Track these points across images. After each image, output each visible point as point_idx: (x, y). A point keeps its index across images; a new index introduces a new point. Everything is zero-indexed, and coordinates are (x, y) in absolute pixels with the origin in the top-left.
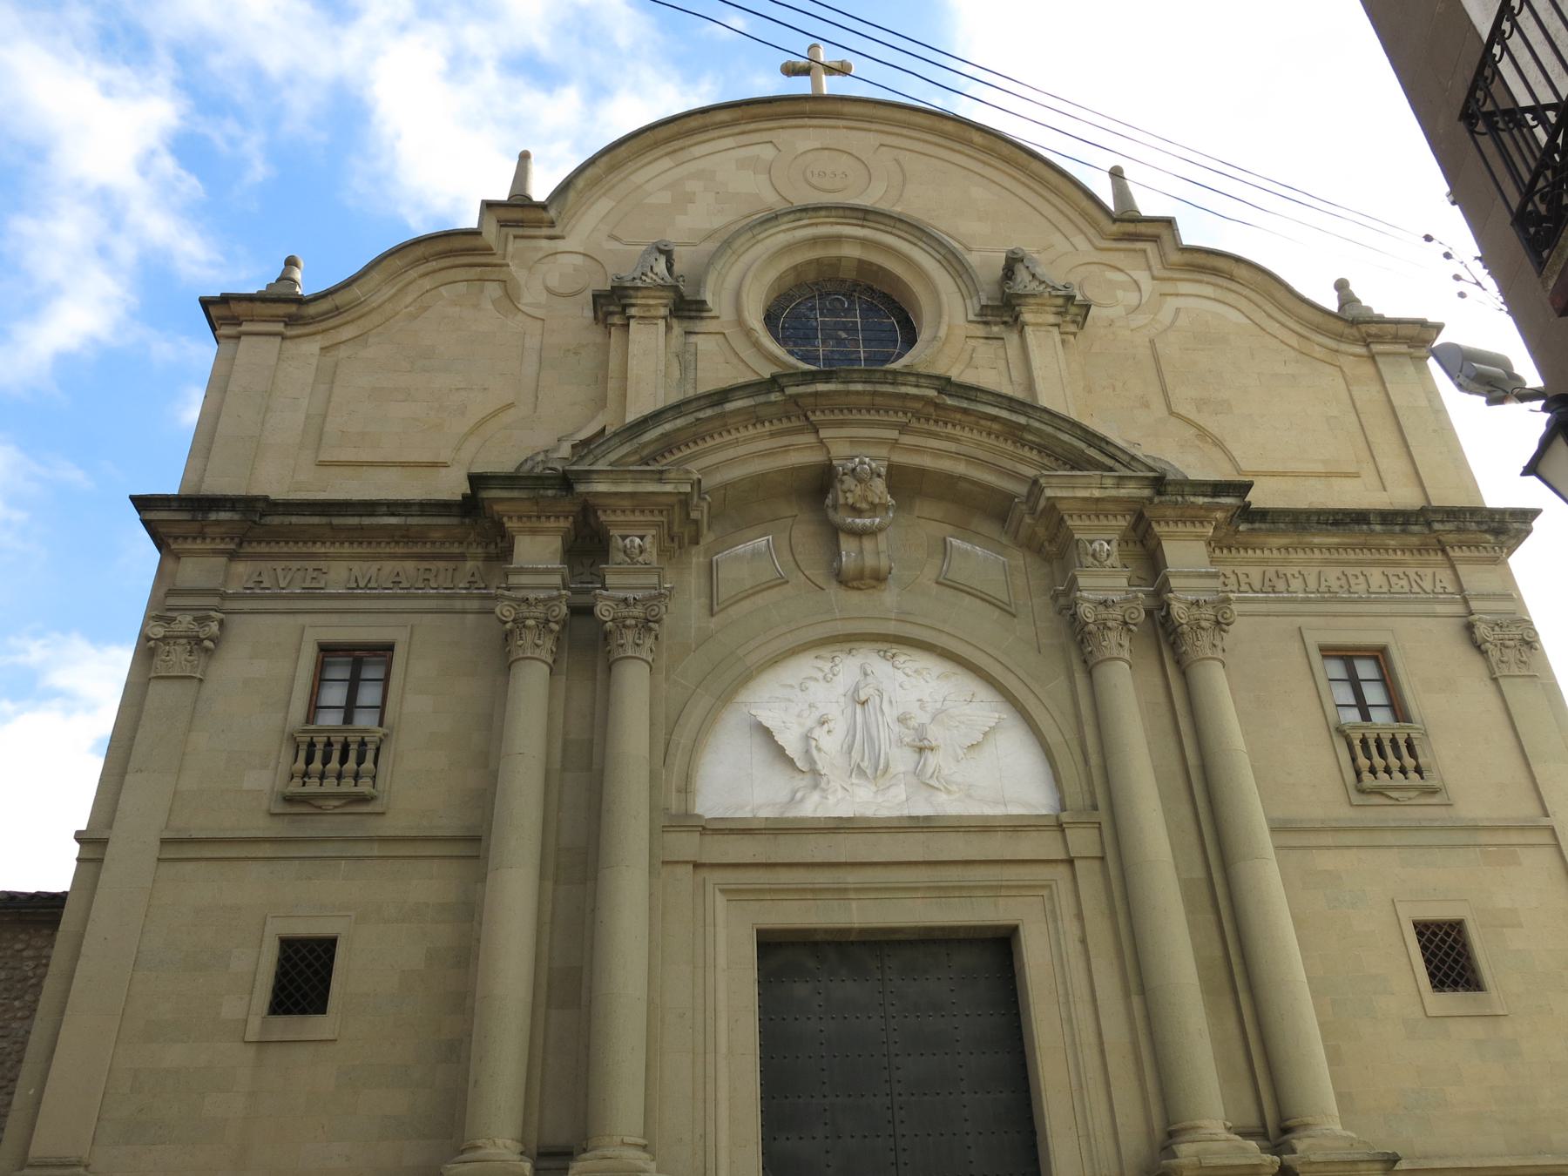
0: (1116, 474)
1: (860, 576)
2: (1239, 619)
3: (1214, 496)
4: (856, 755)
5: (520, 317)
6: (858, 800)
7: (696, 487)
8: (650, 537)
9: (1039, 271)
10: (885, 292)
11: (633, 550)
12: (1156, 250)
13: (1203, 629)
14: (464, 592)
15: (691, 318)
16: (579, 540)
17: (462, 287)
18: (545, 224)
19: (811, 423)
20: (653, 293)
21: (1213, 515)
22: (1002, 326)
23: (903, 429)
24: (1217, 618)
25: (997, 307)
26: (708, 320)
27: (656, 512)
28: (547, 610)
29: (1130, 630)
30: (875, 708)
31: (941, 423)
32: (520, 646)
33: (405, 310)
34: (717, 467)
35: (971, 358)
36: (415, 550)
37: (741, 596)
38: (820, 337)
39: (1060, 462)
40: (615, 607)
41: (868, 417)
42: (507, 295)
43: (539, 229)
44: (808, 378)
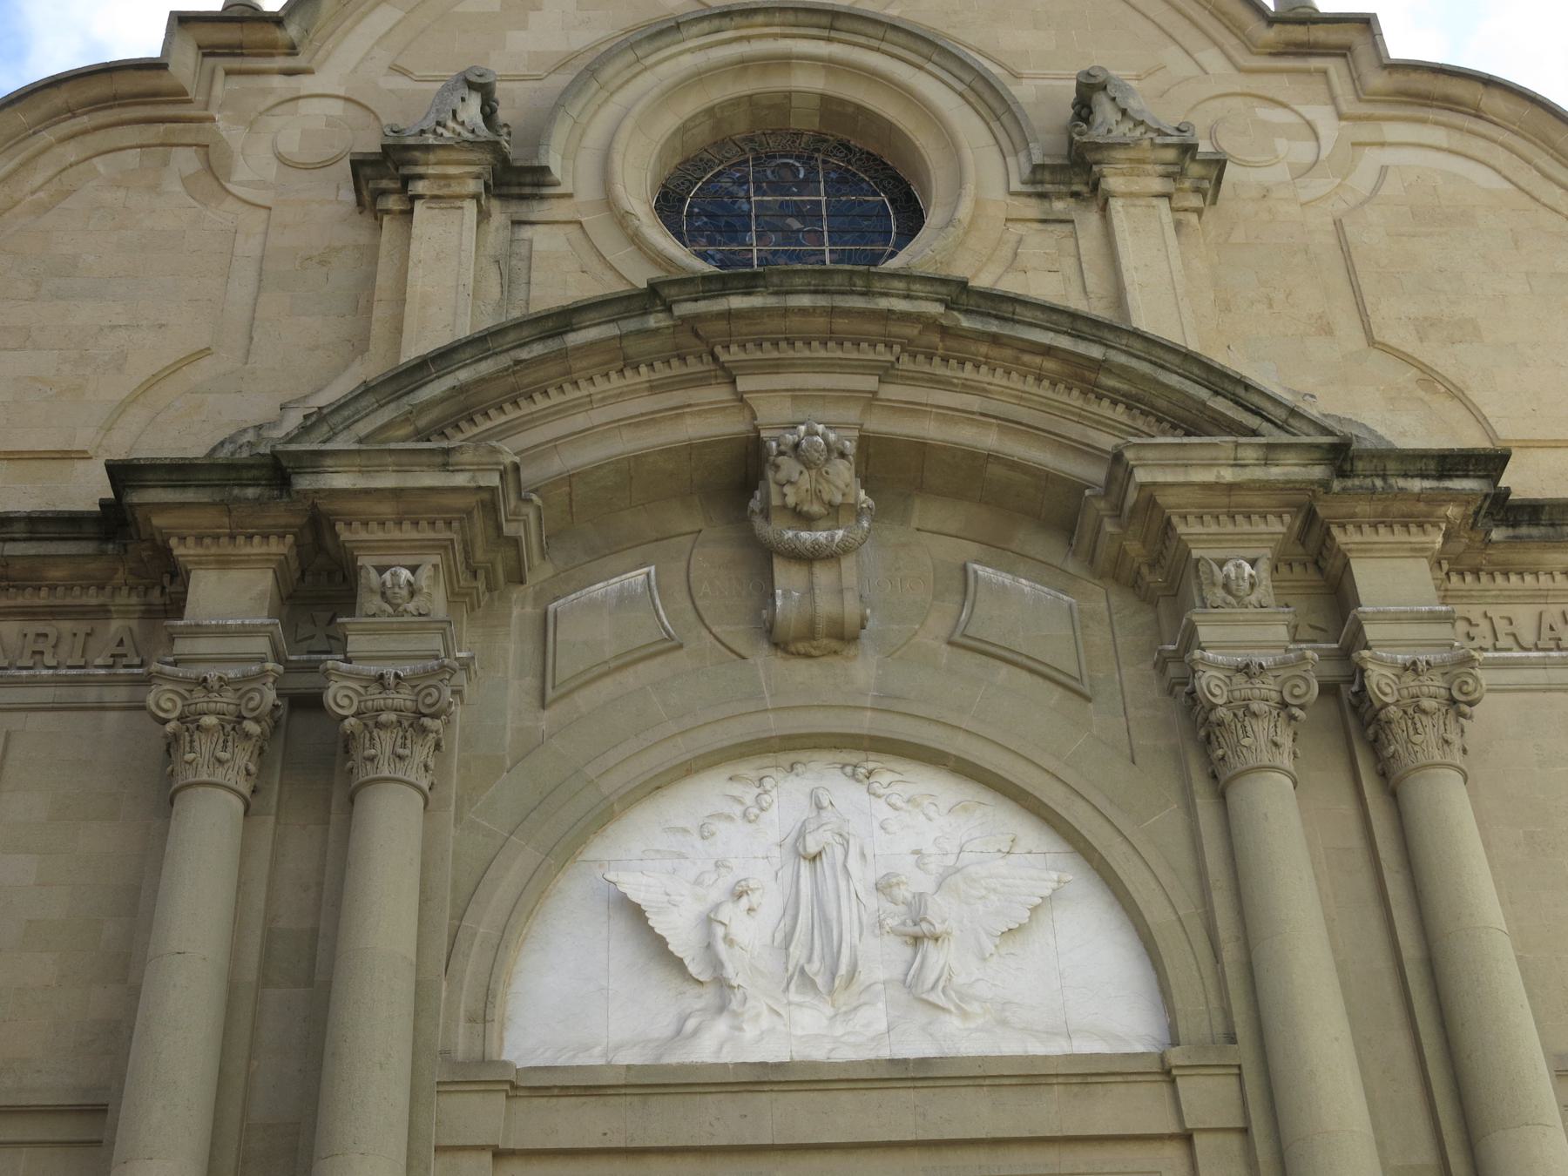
0: (1262, 440)
1: (810, 632)
2: (1488, 697)
3: (1441, 476)
4: (797, 952)
5: (230, 203)
6: (799, 1032)
7: (510, 478)
8: (430, 567)
9: (1133, 104)
10: (871, 151)
11: (397, 590)
12: (1344, 71)
13: (1424, 712)
14: (103, 672)
15: (522, 198)
16: (308, 578)
17: (131, 158)
18: (280, 51)
19: (722, 366)
20: (455, 156)
21: (1441, 511)
22: (1073, 200)
23: (886, 373)
24: (1451, 694)
25: (1062, 168)
26: (554, 202)
27: (440, 524)
28: (241, 698)
29: (1292, 717)
30: (833, 867)
31: (953, 362)
32: (190, 763)
33: (29, 199)
34: (554, 444)
35: (1016, 254)
36: (20, 601)
37: (596, 671)
38: (754, 228)
39: (1166, 425)
40: (362, 690)
41: (823, 354)
42: (209, 168)
43: (269, 59)
44: (713, 287)
